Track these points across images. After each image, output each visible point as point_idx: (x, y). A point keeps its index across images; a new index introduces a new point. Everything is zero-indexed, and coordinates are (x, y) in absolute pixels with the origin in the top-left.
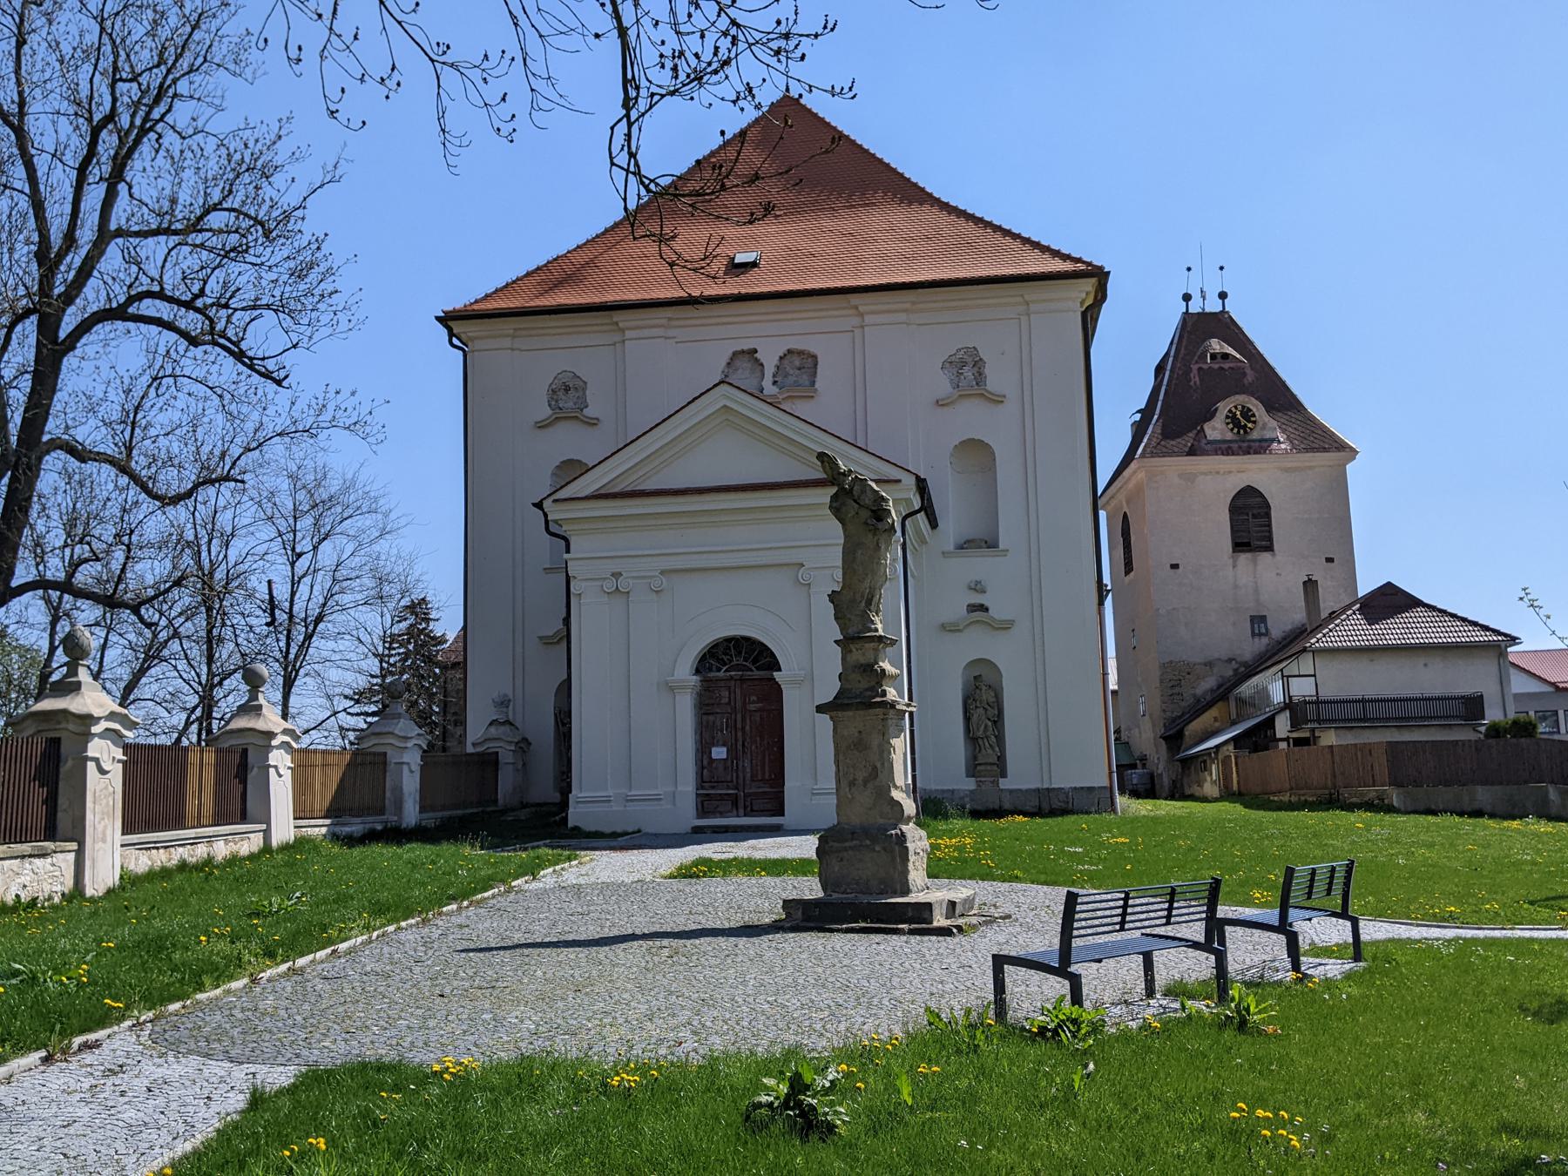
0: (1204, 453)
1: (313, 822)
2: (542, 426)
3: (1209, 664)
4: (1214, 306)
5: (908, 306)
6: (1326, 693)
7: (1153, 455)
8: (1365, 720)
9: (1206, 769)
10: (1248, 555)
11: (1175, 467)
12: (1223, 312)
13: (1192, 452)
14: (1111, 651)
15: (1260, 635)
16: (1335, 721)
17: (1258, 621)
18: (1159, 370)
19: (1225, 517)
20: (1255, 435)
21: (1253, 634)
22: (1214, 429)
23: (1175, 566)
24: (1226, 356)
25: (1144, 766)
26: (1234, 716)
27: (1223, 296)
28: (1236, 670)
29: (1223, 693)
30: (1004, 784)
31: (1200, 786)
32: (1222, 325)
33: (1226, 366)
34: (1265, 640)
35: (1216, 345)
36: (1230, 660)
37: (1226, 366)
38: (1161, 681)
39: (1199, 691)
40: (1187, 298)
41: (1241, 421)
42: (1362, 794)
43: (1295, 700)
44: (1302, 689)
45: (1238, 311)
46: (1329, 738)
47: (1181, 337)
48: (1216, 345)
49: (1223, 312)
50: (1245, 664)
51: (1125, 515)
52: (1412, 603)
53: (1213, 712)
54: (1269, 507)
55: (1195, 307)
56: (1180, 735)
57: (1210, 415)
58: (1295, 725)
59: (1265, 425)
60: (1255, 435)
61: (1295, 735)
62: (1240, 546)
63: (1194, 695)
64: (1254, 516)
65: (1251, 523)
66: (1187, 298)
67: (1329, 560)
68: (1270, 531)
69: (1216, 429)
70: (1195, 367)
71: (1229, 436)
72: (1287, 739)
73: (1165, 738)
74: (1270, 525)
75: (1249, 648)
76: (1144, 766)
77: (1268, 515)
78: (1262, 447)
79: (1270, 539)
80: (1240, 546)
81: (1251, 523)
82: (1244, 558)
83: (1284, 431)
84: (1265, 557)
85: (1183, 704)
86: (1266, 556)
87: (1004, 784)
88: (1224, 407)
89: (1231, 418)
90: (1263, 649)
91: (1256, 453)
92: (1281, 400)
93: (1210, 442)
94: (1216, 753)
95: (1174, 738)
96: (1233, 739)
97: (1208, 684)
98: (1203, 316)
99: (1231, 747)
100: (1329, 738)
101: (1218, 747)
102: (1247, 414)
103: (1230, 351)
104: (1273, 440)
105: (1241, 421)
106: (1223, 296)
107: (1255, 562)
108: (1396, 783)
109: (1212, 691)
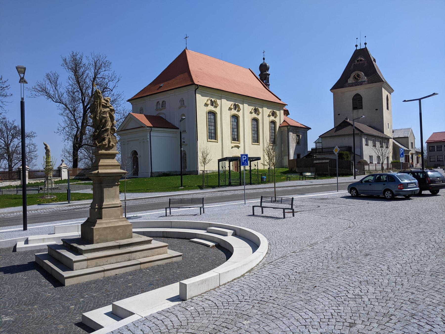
1: (113, 273)
2: (180, 108)
4: (363, 47)
5: (7, 223)
6: (324, 146)
12: (366, 48)
23: (339, 114)
30: (186, 170)
40: (356, 46)
54: (362, 98)
55: (358, 48)
60: (360, 81)
66: (356, 46)
67: (377, 110)
71: (354, 82)
78: (361, 83)
79: (362, 106)
80: (355, 108)
82: (355, 111)
86: (361, 110)
87: (186, 170)
88: (352, 75)
89: (354, 77)
102: (358, 76)
106: (365, 44)
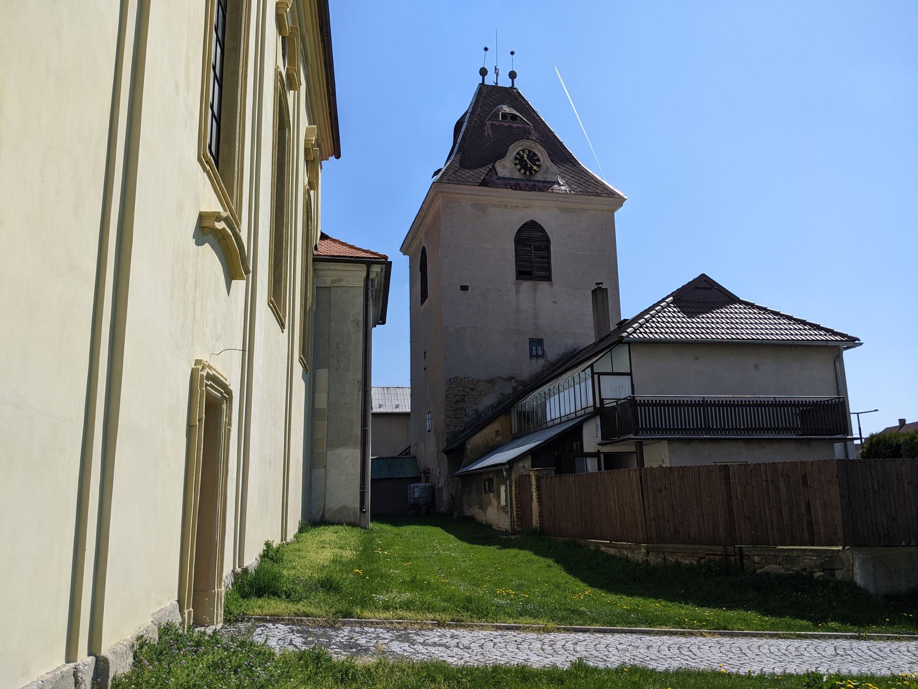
0: (496, 186)
3: (491, 382)
7: (449, 182)
8: (708, 430)
9: (491, 488)
10: (529, 283)
11: (470, 195)
12: (512, 87)
13: (484, 183)
14: (239, 111)
15: (537, 356)
16: (667, 430)
17: (536, 343)
18: (459, 125)
19: (511, 245)
20: (539, 177)
21: (532, 356)
22: (504, 167)
23: (464, 288)
24: (514, 117)
25: (427, 481)
26: (515, 429)
27: (513, 75)
28: (515, 389)
29: (504, 408)
31: (483, 507)
32: (512, 96)
33: (515, 125)
34: (541, 362)
35: (506, 109)
36: (510, 379)
37: (515, 125)
38: (447, 396)
39: (481, 407)
40: (483, 72)
41: (527, 163)
42: (790, 559)
43: (608, 404)
44: (615, 389)
45: (521, 86)
46: (659, 456)
47: (473, 113)
48: (506, 109)
49: (512, 87)
50: (521, 383)
51: (424, 251)
52: (730, 299)
53: (496, 426)
54: (548, 241)
55: (490, 80)
56: (462, 447)
57: (502, 156)
58: (608, 435)
59: (547, 168)
60: (539, 177)
61: (606, 449)
62: (523, 274)
63: (476, 411)
64: (536, 249)
65: (533, 254)
66: (483, 72)
68: (549, 263)
69: (506, 167)
70: (488, 123)
71: (517, 175)
72: (596, 455)
73: (446, 452)
74: (549, 257)
75: (529, 368)
76: (427, 481)
77: (548, 248)
78: (545, 186)
79: (549, 269)
80: (523, 274)
81: (533, 254)
82: (526, 285)
83: (563, 178)
84: (543, 286)
85: (466, 419)
88: (514, 149)
90: (539, 369)
91: (540, 190)
92: (561, 155)
93: (499, 178)
94: (509, 471)
95: (455, 452)
96: (531, 453)
97: (489, 400)
98: (495, 88)
99: (528, 463)
100: (659, 456)
101: (512, 463)
102: (533, 157)
103: (514, 112)
104: (554, 183)
105: (527, 163)
106: (513, 75)
107: (535, 290)
108: (854, 540)
109: (493, 407)
